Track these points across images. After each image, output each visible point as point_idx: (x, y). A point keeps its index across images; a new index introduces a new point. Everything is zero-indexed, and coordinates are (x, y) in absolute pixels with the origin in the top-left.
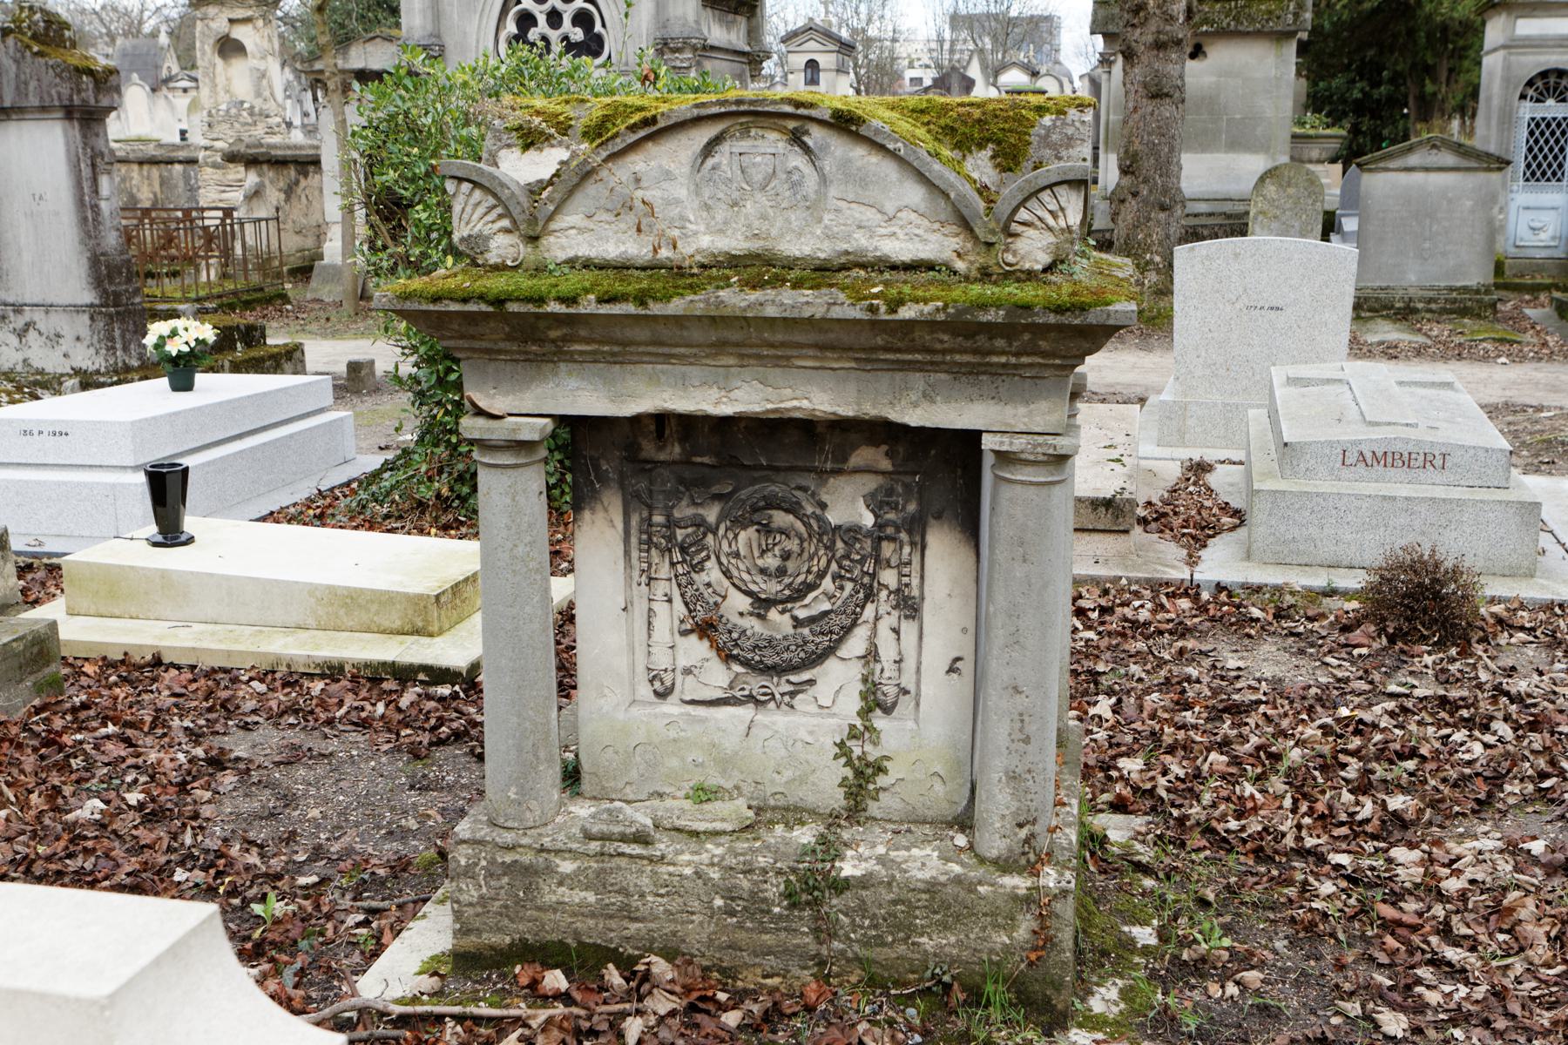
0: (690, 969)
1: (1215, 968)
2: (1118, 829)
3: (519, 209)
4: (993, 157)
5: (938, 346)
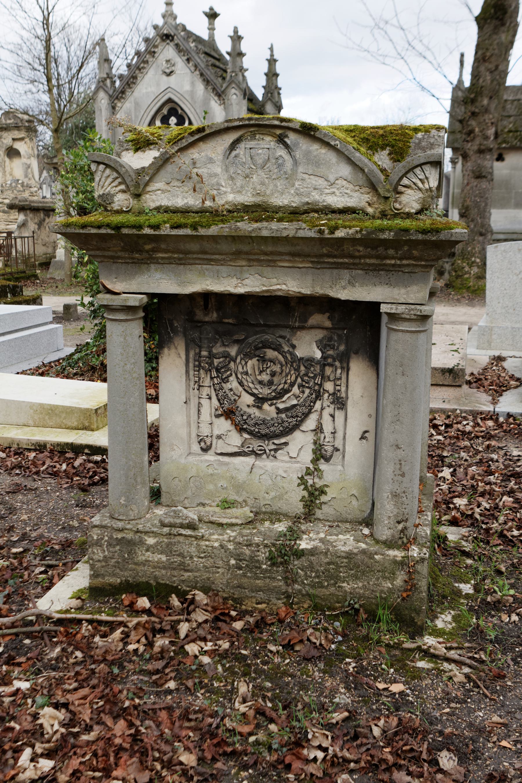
0: (217, 598)
1: (505, 606)
2: (453, 534)
3: (130, 179)
4: (389, 154)
5: (357, 254)
